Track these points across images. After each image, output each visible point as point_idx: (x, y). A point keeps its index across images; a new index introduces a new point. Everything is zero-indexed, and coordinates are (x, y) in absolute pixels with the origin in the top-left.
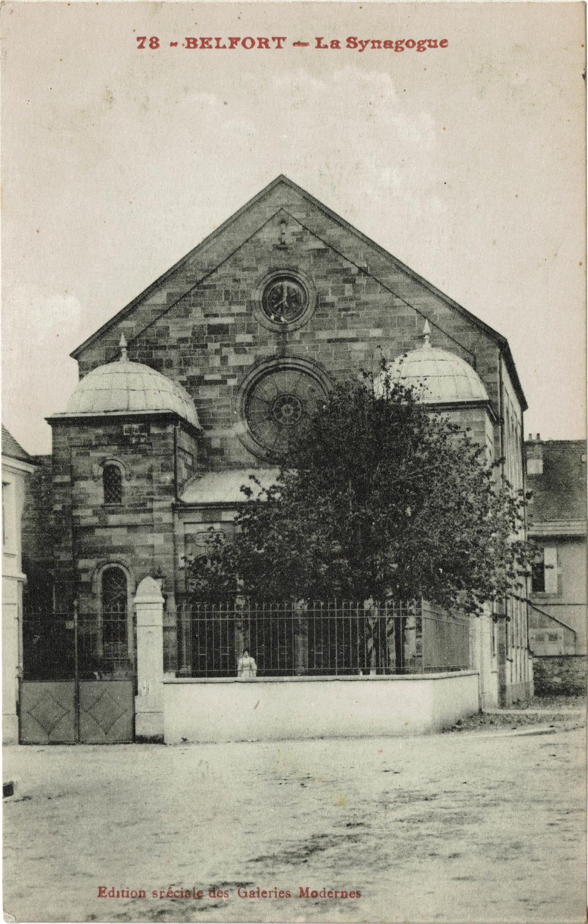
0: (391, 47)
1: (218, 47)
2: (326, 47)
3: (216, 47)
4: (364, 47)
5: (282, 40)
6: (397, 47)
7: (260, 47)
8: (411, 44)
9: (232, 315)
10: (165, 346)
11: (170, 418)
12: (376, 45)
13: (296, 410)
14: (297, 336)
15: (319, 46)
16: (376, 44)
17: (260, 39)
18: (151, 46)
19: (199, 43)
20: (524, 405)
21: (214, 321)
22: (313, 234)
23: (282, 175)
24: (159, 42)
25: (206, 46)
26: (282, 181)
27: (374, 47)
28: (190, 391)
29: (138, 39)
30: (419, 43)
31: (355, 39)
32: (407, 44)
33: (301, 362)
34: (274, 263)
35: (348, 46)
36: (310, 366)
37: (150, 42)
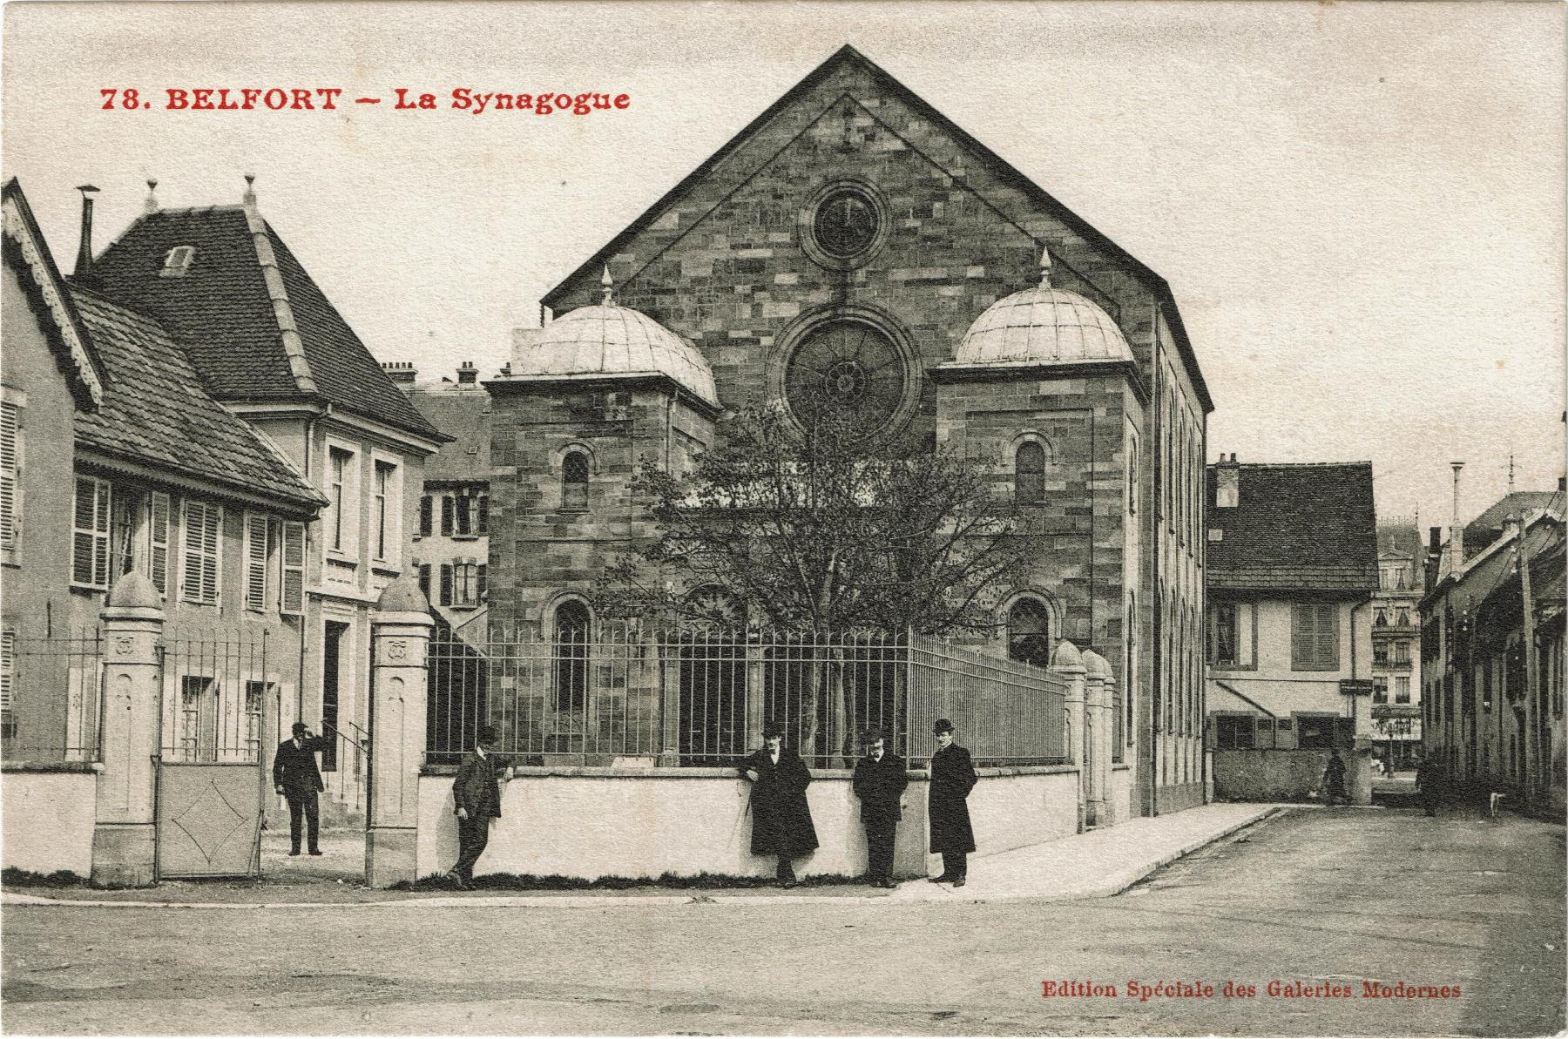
0: (529, 106)
1: (223, 106)
2: (413, 106)
3: (220, 107)
4: (483, 105)
5: (333, 95)
6: (539, 106)
7: (296, 106)
8: (563, 102)
9: (769, 246)
10: (674, 290)
11: (661, 384)
12: (505, 102)
13: (858, 383)
14: (861, 276)
15: (401, 106)
16: (503, 101)
17: (296, 92)
18: (125, 104)
19: (191, 99)
20: (1208, 406)
21: (744, 254)
22: (889, 129)
23: (847, 46)
24: (124, 98)
25: (202, 103)
26: (847, 58)
27: (499, 106)
28: (705, 355)
29: (104, 92)
30: (577, 99)
31: (467, 92)
32: (557, 102)
33: (869, 315)
34: (833, 170)
35: (456, 105)
36: (879, 319)
37: (124, 98)
